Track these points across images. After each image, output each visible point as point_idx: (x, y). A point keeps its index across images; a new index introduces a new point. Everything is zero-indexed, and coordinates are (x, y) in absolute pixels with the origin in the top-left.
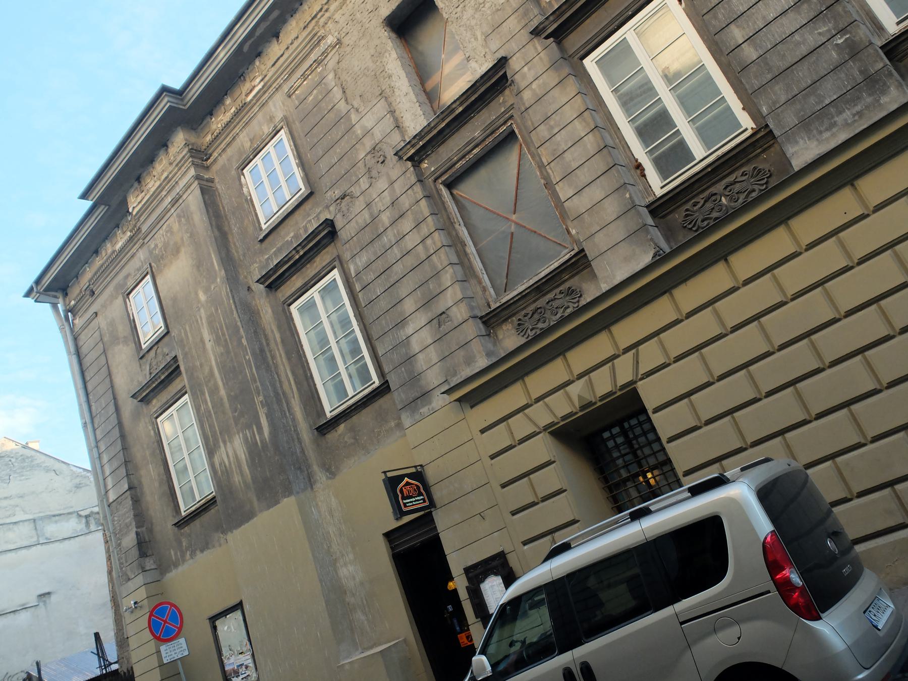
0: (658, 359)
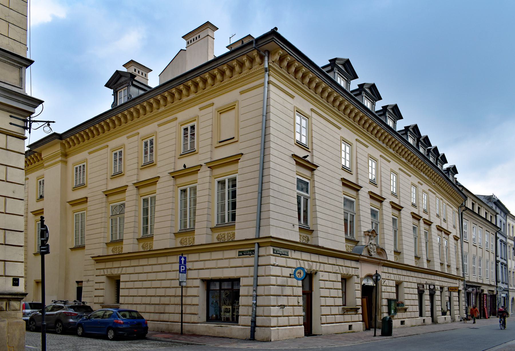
0: (127, 272)
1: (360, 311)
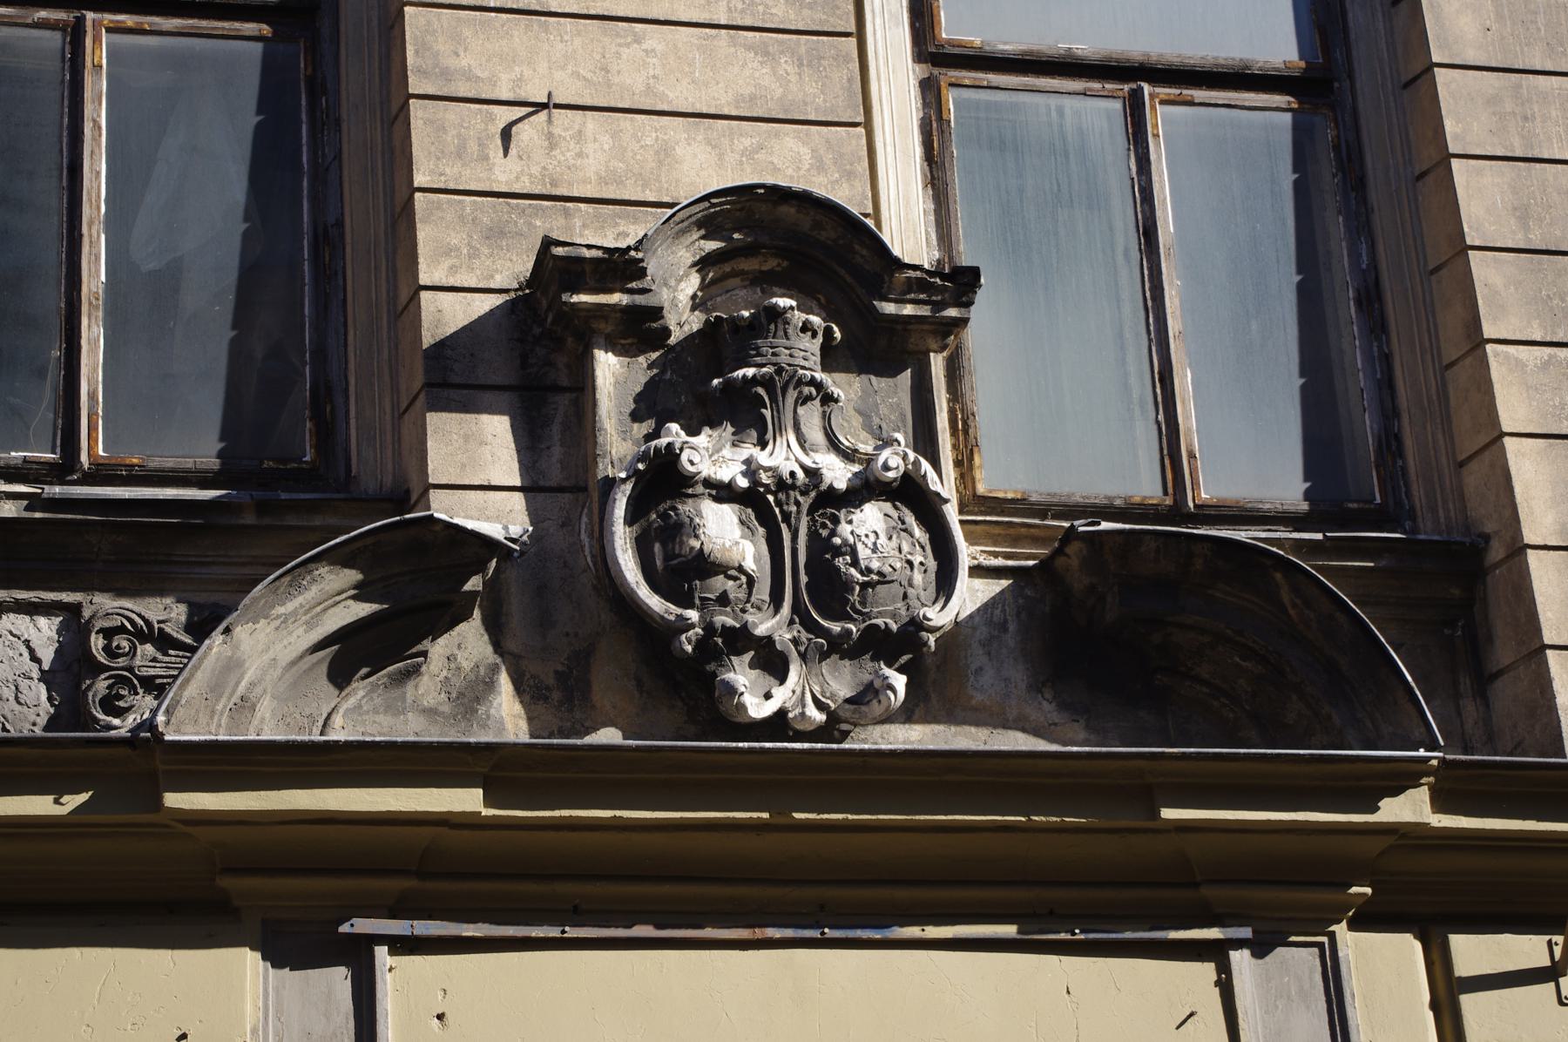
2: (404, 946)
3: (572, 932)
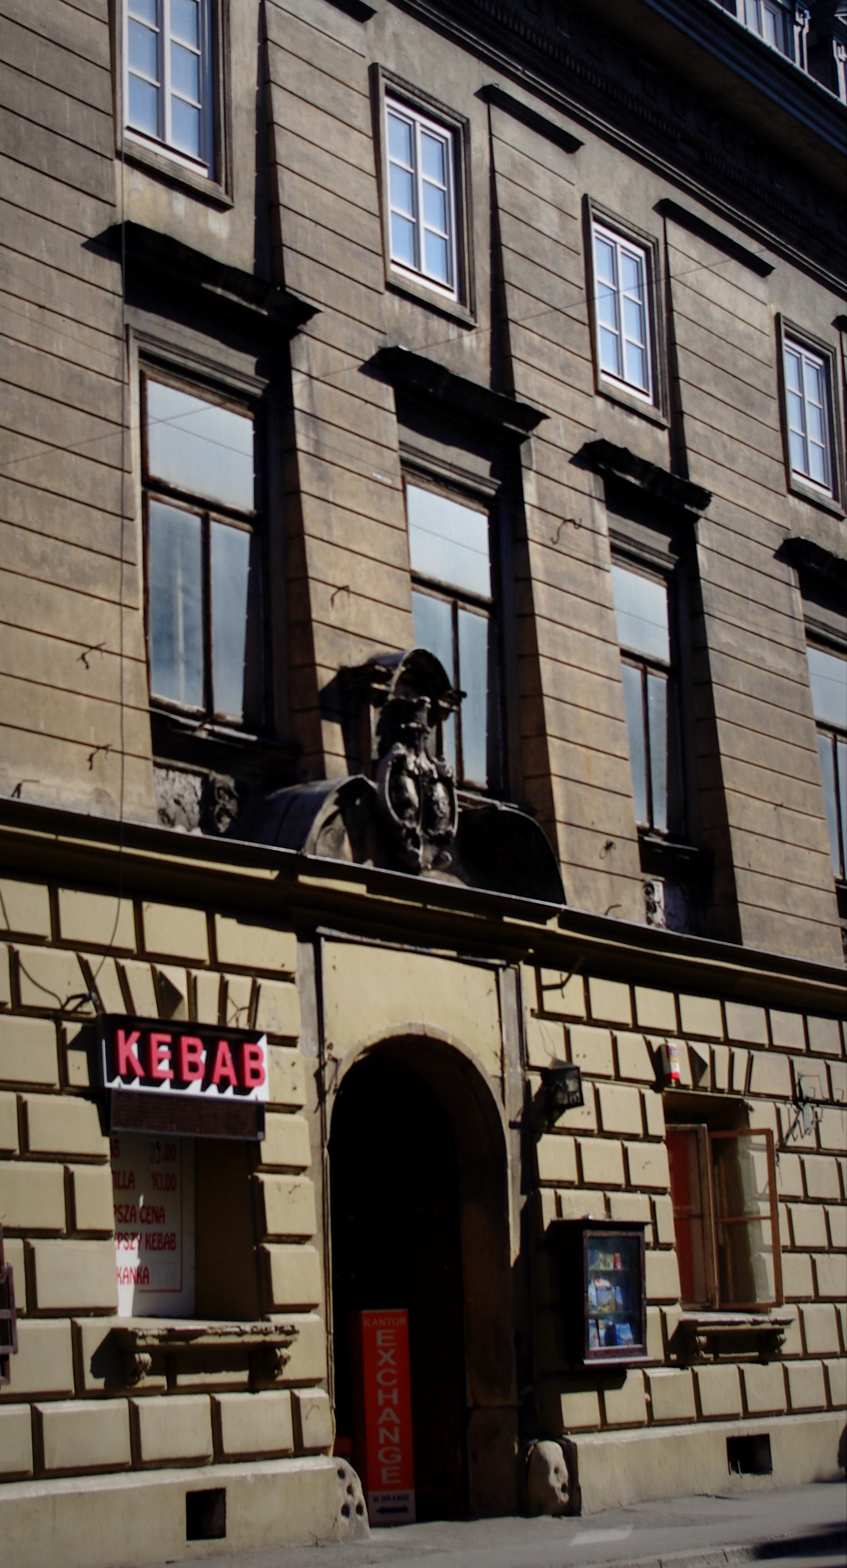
1: (309, 1350)
2: (330, 939)
3: (419, 949)
